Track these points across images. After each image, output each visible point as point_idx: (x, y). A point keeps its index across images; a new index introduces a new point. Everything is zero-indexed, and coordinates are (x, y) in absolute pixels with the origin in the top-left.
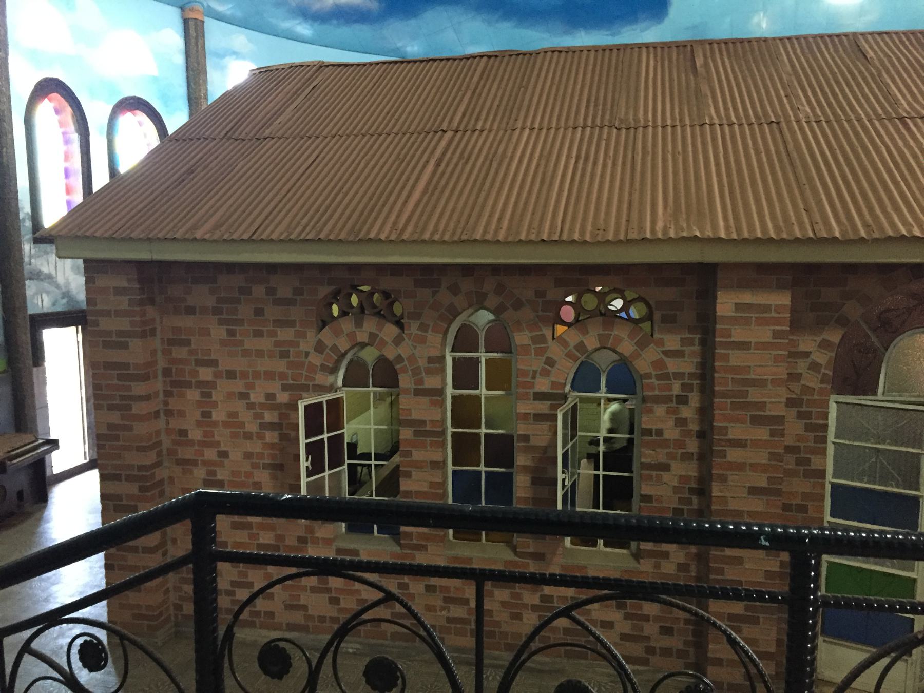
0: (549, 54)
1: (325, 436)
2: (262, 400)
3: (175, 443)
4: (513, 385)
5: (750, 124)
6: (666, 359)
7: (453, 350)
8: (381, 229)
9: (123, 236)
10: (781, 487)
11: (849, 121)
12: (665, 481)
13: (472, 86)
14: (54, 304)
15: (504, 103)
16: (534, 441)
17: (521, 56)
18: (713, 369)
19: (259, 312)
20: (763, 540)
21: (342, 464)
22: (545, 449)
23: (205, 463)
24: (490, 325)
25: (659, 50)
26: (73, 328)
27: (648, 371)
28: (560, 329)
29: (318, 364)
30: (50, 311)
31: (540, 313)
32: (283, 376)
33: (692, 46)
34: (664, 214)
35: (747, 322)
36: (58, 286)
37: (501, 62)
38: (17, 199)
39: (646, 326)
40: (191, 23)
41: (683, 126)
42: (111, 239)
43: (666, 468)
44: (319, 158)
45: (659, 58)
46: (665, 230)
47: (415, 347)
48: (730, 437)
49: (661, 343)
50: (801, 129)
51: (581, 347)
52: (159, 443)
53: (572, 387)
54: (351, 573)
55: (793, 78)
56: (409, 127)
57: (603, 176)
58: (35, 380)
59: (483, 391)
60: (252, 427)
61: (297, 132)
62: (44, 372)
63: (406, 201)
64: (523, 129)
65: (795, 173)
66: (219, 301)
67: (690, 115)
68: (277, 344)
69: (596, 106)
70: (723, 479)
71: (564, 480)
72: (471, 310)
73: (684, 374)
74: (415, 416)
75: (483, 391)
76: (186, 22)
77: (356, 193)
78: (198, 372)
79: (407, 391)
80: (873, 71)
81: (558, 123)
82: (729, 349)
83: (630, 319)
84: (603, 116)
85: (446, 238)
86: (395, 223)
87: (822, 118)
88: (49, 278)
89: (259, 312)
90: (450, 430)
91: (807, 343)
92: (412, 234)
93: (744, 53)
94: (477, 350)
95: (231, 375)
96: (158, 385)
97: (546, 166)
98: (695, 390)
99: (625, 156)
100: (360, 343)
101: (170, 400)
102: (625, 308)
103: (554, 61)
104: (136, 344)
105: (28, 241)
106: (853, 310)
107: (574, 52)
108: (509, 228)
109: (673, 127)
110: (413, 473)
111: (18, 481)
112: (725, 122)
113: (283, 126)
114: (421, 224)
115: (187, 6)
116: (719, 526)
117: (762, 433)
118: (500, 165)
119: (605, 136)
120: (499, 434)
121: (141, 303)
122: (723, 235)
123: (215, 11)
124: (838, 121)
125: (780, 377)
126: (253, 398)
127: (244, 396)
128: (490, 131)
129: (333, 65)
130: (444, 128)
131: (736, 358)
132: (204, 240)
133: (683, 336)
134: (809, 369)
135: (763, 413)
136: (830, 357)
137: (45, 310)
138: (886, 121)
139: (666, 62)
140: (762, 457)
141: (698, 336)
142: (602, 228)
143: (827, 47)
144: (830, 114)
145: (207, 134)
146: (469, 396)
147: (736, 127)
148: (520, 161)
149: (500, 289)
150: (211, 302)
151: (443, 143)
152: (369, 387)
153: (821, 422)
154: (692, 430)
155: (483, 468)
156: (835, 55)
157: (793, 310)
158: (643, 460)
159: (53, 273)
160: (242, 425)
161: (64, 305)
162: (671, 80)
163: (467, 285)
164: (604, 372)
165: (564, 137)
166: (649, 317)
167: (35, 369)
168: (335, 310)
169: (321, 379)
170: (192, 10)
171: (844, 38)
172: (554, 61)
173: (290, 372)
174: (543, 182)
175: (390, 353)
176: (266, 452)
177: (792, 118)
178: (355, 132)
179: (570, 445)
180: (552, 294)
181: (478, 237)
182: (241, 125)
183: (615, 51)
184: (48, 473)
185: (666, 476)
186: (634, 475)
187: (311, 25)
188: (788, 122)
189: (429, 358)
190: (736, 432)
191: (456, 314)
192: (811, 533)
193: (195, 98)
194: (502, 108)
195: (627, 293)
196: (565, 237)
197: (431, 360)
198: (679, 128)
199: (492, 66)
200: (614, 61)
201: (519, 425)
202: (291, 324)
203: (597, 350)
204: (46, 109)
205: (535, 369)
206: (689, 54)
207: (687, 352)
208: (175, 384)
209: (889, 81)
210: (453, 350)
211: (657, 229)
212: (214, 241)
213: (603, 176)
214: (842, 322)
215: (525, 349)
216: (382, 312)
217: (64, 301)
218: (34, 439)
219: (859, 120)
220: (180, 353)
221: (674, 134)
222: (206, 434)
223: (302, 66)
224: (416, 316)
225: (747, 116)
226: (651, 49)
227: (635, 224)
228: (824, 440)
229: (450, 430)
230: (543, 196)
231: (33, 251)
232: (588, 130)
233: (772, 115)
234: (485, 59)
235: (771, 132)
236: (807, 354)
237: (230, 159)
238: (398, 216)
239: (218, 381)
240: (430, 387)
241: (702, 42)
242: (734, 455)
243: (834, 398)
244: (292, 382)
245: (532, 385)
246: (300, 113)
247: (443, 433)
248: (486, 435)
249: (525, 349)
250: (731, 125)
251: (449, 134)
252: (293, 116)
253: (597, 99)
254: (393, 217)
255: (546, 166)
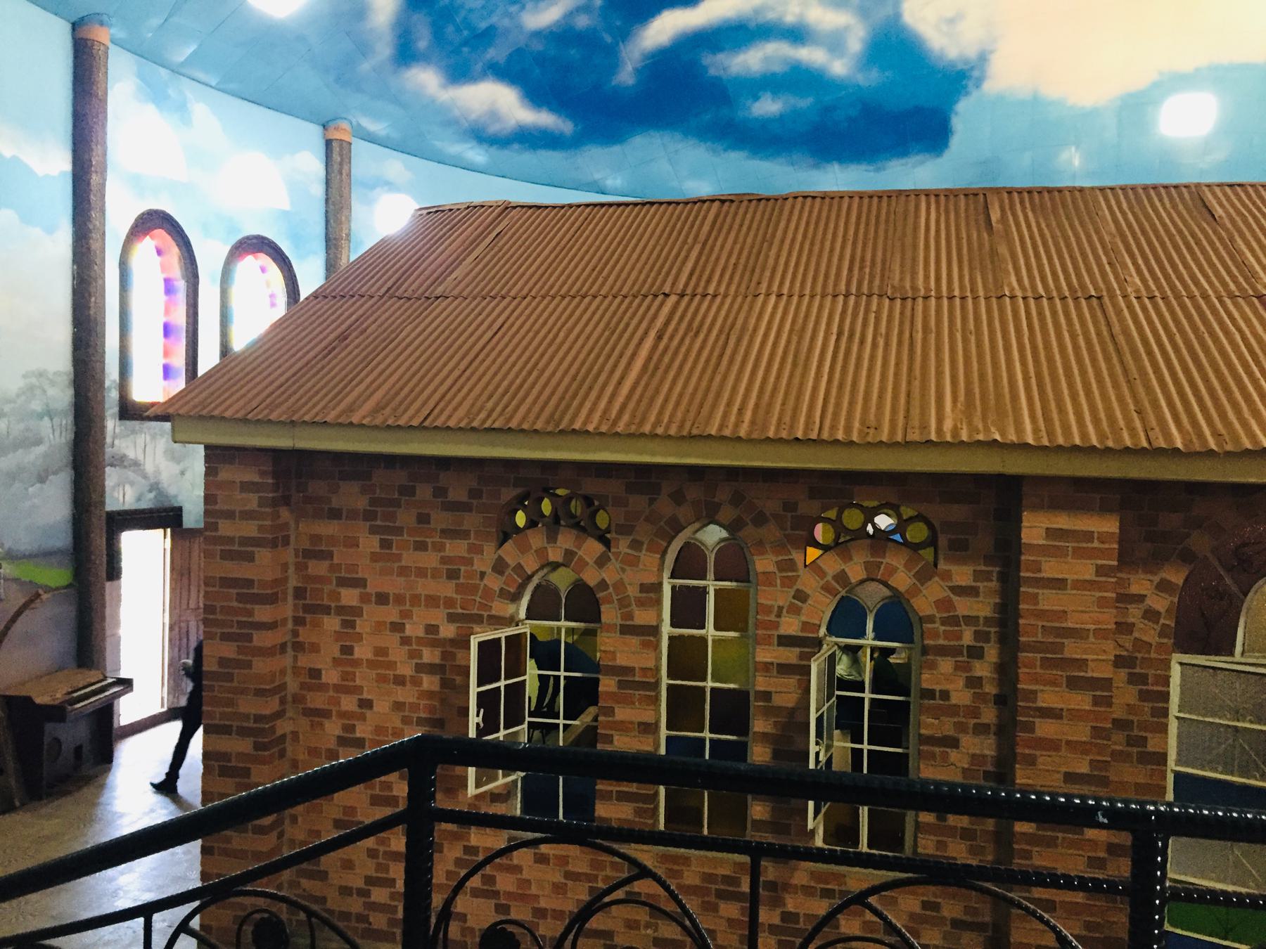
0: (800, 199)
1: (502, 684)
2: (421, 633)
3: (303, 686)
4: (751, 622)
5: (1063, 299)
6: (955, 598)
7: (673, 576)
8: (588, 417)
9: (259, 417)
10: (1108, 774)
11: (1192, 298)
12: (952, 760)
13: (702, 237)
14: (139, 499)
15: (742, 261)
16: (777, 701)
17: (763, 202)
18: (1017, 615)
19: (423, 519)
20: (1101, 817)
21: (522, 723)
22: (792, 712)
23: (343, 715)
24: (722, 544)
25: (942, 198)
26: (161, 531)
27: (928, 613)
28: (813, 553)
29: (497, 589)
30: (134, 507)
31: (789, 531)
32: (449, 603)
33: (985, 195)
34: (953, 411)
35: (1058, 553)
36: (145, 477)
37: (738, 208)
38: (103, 362)
39: (928, 554)
40: (334, 144)
41: (975, 298)
42: (245, 421)
43: (953, 743)
44: (506, 326)
45: (942, 208)
46: (955, 432)
47: (623, 570)
48: (1040, 704)
49: (947, 576)
50: (1130, 307)
51: (842, 577)
52: (283, 687)
53: (828, 629)
54: (599, 841)
55: (1118, 240)
56: (621, 289)
57: (872, 358)
58: (107, 598)
59: (710, 631)
60: (407, 670)
61: (477, 290)
62: (119, 588)
63: (619, 383)
64: (768, 295)
65: (1122, 362)
66: (373, 502)
67: (985, 286)
68: (444, 560)
69: (861, 268)
70: (1031, 761)
71: (817, 754)
72: (697, 525)
73: (977, 617)
74: (621, 661)
75: (710, 631)
76: (328, 143)
77: (436, 329)
78: (339, 593)
79: (610, 628)
80: (1223, 234)
81: (813, 288)
82: (1038, 588)
83: (906, 544)
84: (871, 282)
85: (672, 432)
86: (606, 411)
87: (1157, 294)
88: (136, 464)
89: (423, 519)
90: (665, 681)
91: (1140, 584)
92: (628, 425)
93: (1055, 210)
94: (703, 578)
95: (382, 599)
96: (287, 609)
97: (799, 343)
98: (992, 640)
99: (901, 333)
100: (552, 562)
101: (301, 630)
102: (900, 527)
103: (807, 209)
104: (263, 555)
105: (112, 416)
106: (1200, 543)
107: (832, 198)
108: (753, 422)
109: (963, 298)
110: (616, 738)
111: (73, 734)
112: (1029, 294)
113: (460, 282)
114: (639, 415)
115: (331, 124)
116: (1048, 798)
117: (1081, 701)
118: (739, 340)
119: (874, 308)
120: (729, 690)
121: (275, 503)
122: (1031, 441)
123: (363, 129)
124: (1178, 297)
125: (1105, 627)
126: (409, 630)
127: (397, 627)
128: (725, 296)
129: (523, 207)
130: (667, 289)
131: (1048, 600)
132: (362, 426)
133: (978, 568)
134: (1143, 618)
135: (1082, 674)
136: (1172, 602)
137: (127, 507)
138: (1240, 300)
139: (952, 216)
140: (1081, 733)
141: (998, 569)
142: (873, 424)
143: (1161, 200)
144: (1167, 289)
145: (364, 289)
146: (692, 637)
147: (1045, 301)
148: (766, 335)
149: (737, 500)
150: (362, 503)
151: (666, 310)
152: (560, 620)
153: (1160, 688)
154: (988, 693)
155: (707, 734)
156: (1172, 211)
157: (1123, 538)
158: (923, 731)
159: (141, 457)
160: (391, 665)
161: (150, 500)
162: (959, 239)
163: (694, 492)
164: (871, 611)
165: (821, 307)
166: (932, 542)
167: (108, 584)
168: (521, 519)
169: (502, 608)
170: (336, 129)
171: (1184, 190)
172: (807, 209)
173: (459, 597)
174: (795, 365)
175: (591, 577)
176: (422, 702)
177: (1118, 292)
178: (552, 293)
179: (825, 708)
180: (807, 507)
181: (713, 433)
182: (406, 280)
183: (885, 199)
184: (115, 725)
185: (953, 755)
186: (912, 751)
187: (487, 151)
188: (1112, 297)
189: (641, 585)
190: (1048, 698)
191: (678, 529)
192: (1157, 810)
193: (335, 239)
194: (740, 267)
195: (903, 509)
196: (825, 436)
197: (644, 588)
198: (970, 301)
199: (727, 213)
200: (884, 212)
201: (758, 678)
202: (464, 535)
203: (862, 582)
204: (145, 248)
205: (781, 604)
206: (981, 208)
207: (981, 590)
208: (309, 609)
209: (1243, 247)
210: (673, 576)
211: (945, 429)
212: (376, 427)
213: (872, 358)
214: (1187, 557)
215: (768, 578)
216: (582, 523)
217: (152, 495)
218: (101, 677)
219: (1206, 297)
220: (318, 568)
221: (963, 308)
222: (346, 676)
223: (483, 206)
224: (625, 530)
225: (1059, 288)
226: (933, 199)
227: (916, 422)
228: (1165, 713)
229: (665, 681)
230: (796, 381)
231: (117, 430)
232: (852, 299)
233: (1091, 287)
234: (717, 204)
235: (1091, 308)
236: (1141, 598)
237: (393, 323)
238: (610, 402)
239: (366, 608)
240: (642, 623)
241: (997, 191)
242: (1045, 728)
243: (1177, 657)
244: (460, 611)
245: (776, 625)
246: (480, 266)
247: (657, 684)
248: (713, 689)
249: (768, 578)
250: (1038, 298)
251: (673, 298)
252: (471, 271)
253: (863, 260)
254: (602, 404)
255: (799, 343)
